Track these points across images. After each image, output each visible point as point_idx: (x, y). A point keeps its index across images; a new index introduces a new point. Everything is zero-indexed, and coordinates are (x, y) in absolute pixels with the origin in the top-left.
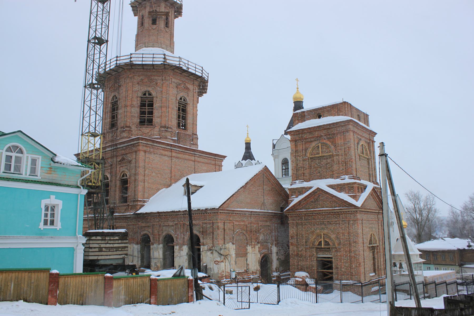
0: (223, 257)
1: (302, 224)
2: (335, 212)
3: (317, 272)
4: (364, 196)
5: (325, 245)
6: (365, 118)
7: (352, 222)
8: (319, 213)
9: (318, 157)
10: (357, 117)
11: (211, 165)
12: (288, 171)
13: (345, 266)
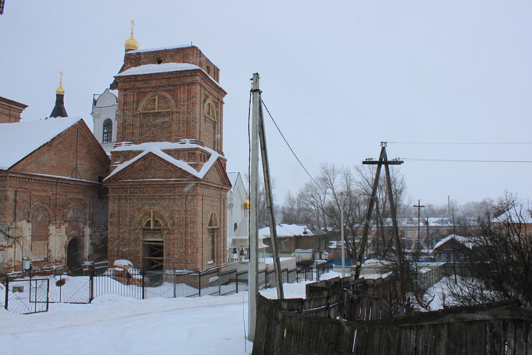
0: (11, 240)
1: (126, 199)
2: (170, 185)
3: (143, 259)
4: (207, 166)
5: (155, 225)
6: (216, 72)
7: (190, 197)
8: (150, 185)
9: (153, 113)
10: (206, 68)
11: (4, 116)
12: (111, 136)
13: (179, 252)
